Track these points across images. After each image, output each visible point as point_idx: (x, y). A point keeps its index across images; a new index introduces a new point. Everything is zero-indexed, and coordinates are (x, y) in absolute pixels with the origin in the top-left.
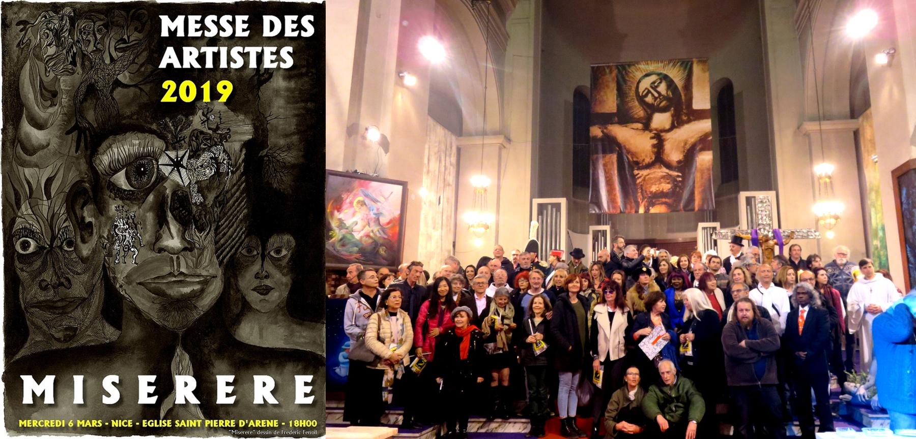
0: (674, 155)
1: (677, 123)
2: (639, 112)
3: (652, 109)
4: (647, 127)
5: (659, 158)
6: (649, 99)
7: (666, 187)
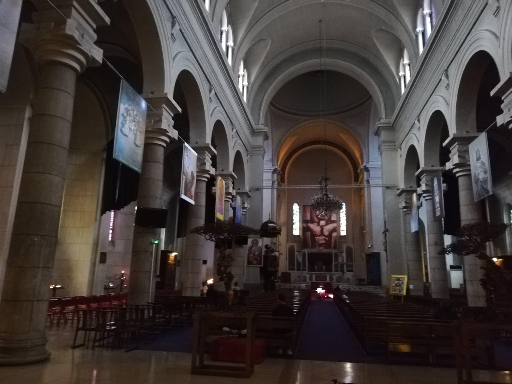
0: (326, 233)
1: (327, 224)
2: (316, 220)
3: (320, 219)
4: (319, 225)
5: (322, 233)
6: (319, 216)
7: (324, 242)
